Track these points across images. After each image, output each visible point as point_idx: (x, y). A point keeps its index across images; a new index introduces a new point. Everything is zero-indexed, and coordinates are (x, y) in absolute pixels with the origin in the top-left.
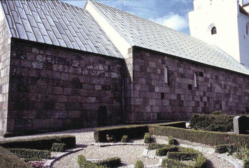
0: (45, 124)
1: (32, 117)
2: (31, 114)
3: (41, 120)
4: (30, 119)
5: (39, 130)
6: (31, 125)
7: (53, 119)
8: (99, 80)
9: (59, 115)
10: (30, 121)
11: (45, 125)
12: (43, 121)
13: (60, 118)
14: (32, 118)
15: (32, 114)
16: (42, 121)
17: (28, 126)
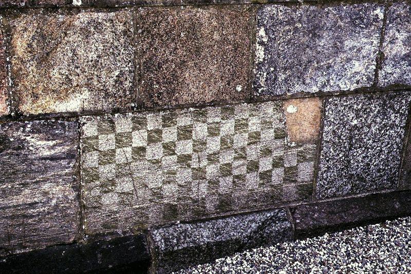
0: (227, 158)
1: (68, 88)
2: (44, 60)
3: (184, 121)
4: (49, 124)
5: (158, 236)
6: (58, 191)
7: (311, 108)
8: (214, 248)
9: (381, 60)
10: (42, 146)
11: (226, 170)
12: (200, 130)
13: (382, 91)
14: (73, 104)
15: (62, 56)
16: (186, 133)
17: (19, 200)
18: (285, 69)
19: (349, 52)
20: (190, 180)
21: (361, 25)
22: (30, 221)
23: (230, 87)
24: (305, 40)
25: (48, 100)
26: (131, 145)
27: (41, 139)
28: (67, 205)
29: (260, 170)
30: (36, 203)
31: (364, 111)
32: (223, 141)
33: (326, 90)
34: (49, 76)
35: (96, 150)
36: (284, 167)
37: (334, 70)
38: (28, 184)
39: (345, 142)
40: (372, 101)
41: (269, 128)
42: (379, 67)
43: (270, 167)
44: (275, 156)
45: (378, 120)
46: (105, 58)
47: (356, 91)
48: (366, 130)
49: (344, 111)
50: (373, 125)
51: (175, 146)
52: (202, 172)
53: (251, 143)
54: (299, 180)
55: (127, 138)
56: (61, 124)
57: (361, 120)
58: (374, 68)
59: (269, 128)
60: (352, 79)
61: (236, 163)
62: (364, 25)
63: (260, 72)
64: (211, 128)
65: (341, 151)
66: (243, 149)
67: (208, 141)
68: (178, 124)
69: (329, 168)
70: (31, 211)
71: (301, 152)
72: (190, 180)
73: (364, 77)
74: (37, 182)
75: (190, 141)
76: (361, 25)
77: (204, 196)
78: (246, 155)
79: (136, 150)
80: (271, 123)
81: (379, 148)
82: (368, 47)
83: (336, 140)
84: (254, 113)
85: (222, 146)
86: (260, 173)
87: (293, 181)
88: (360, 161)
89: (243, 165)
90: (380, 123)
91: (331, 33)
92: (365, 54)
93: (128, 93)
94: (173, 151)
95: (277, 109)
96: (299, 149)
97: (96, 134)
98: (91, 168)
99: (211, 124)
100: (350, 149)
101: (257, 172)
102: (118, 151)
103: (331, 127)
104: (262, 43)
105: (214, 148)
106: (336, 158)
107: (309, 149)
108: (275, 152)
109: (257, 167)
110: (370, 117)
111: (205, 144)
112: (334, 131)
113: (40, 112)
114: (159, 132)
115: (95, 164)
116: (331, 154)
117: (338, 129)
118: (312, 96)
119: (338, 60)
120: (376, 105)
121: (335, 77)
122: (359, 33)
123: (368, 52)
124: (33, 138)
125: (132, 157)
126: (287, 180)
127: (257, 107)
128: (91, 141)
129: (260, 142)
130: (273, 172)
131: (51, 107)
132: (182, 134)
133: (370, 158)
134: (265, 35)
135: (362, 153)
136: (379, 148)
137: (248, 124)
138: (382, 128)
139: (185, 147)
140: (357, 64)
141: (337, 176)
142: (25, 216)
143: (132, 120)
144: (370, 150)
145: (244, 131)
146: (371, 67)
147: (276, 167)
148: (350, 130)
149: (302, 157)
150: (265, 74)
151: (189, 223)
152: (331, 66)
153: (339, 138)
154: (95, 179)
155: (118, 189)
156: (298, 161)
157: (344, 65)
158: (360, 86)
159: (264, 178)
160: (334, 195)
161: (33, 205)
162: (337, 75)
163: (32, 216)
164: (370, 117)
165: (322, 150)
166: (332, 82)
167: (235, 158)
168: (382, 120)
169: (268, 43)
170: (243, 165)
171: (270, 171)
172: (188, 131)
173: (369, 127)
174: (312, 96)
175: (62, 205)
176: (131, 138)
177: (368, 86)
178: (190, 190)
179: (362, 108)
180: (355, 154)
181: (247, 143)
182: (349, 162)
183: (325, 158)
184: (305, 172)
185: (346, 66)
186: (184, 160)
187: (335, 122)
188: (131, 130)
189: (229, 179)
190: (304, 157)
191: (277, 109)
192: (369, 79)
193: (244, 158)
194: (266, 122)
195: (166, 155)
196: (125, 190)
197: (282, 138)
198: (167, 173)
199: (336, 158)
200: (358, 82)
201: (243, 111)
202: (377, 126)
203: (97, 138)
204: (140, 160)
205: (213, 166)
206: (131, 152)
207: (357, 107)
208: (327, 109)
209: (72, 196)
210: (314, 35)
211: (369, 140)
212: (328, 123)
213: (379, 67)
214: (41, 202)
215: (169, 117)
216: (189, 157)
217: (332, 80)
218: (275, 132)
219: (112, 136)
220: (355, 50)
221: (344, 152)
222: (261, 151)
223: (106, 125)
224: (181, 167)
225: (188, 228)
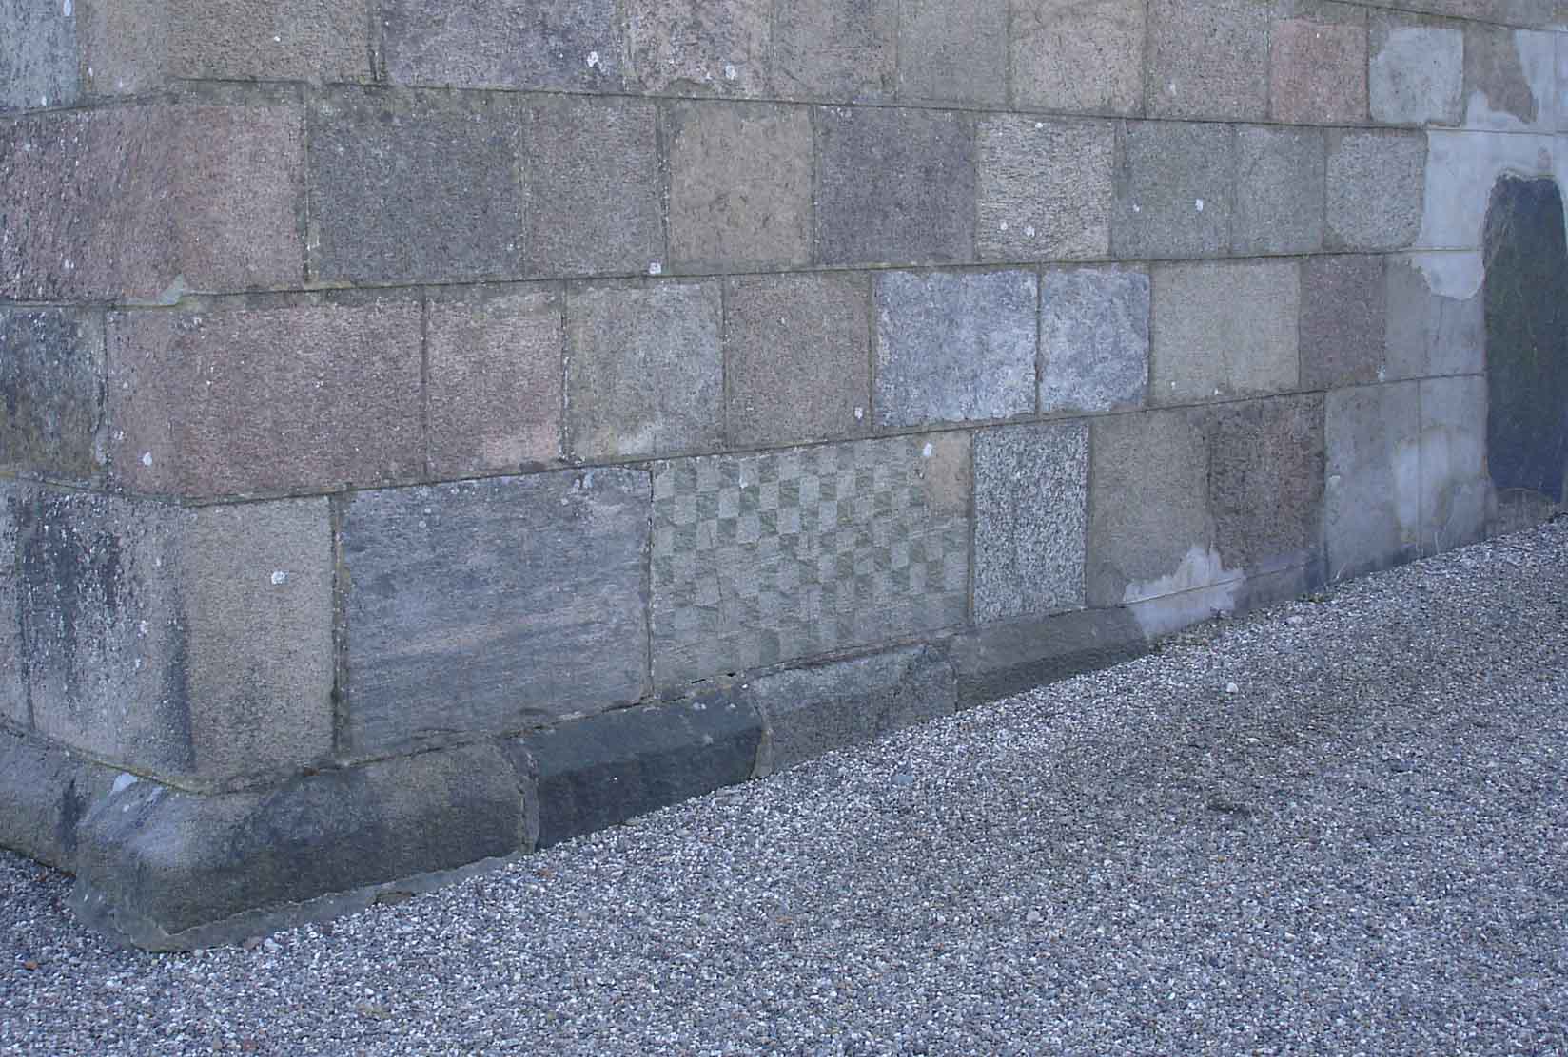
7: (955, 446)
22: (581, 657)
70: (583, 637)
167: (857, 543)
173: (1037, 484)
192: (1029, 399)
210: (952, 321)
223: (685, 477)
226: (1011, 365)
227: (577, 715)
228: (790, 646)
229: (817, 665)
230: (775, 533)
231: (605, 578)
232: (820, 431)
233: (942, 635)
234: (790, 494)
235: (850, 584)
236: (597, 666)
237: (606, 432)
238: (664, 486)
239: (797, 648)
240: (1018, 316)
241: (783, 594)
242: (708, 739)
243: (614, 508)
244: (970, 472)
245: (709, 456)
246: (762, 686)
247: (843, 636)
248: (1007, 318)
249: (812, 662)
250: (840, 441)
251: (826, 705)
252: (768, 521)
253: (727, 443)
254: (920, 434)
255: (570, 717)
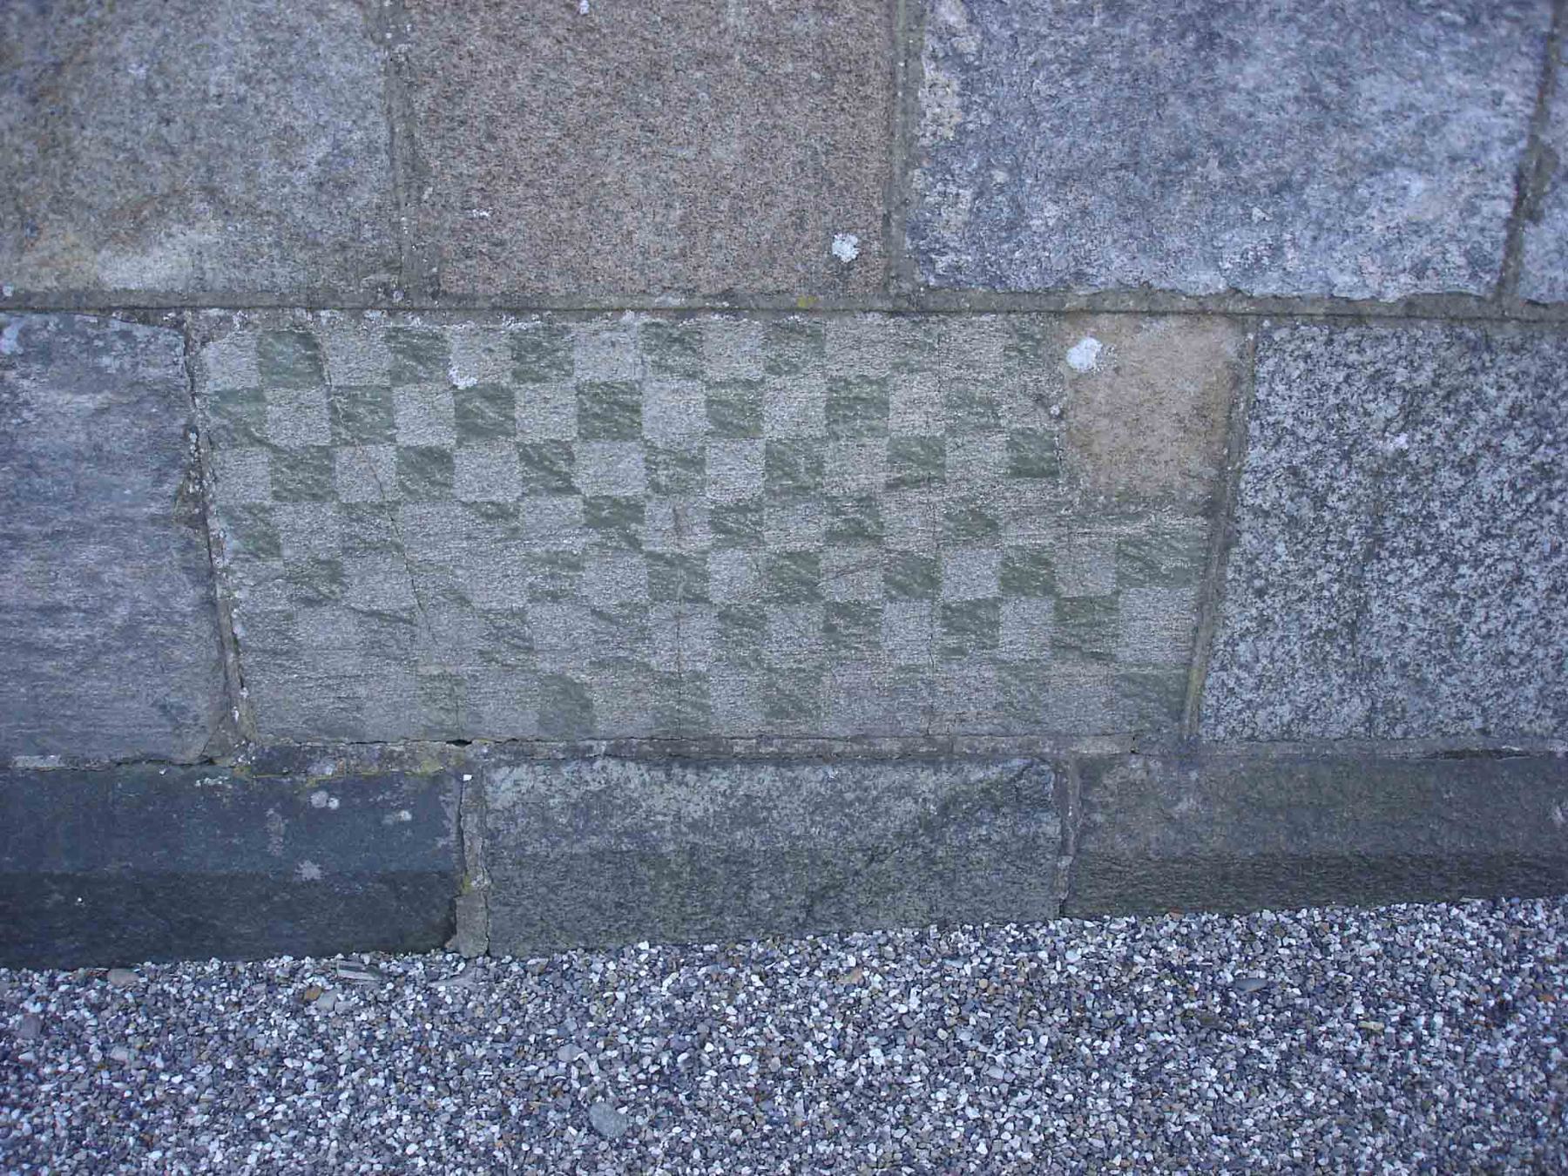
0: (800, 530)
7: (1185, 360)
18: (1065, 179)
19: (1381, 128)
20: (643, 598)
21: (1443, 13)
22: (48, 666)
23: (806, 238)
24: (1166, 56)
25: (72, 238)
26: (392, 439)
27: (61, 386)
28: (168, 630)
29: (947, 594)
30: (60, 608)
31: (1447, 397)
32: (776, 461)
33: (1268, 285)
34: (68, 151)
35: (260, 442)
36: (1058, 595)
37: (1304, 205)
38: (25, 537)
39: (1346, 524)
40: (1486, 357)
41: (983, 427)
42: (1526, 210)
43: (992, 589)
44: (1018, 548)
45: (1512, 443)
46: (272, 88)
47: (1411, 310)
48: (1450, 480)
49: (1345, 388)
50: (1486, 461)
51: (571, 459)
52: (692, 572)
53: (902, 481)
54: (1126, 654)
55: (374, 407)
56: (125, 335)
57: (1430, 437)
58: (1505, 209)
59: (983, 427)
60: (1394, 251)
61: (836, 556)
62: (1461, 12)
63: (940, 187)
64: (720, 402)
65: (1328, 558)
66: (866, 501)
67: (710, 453)
68: (578, 373)
69: (1264, 621)
70: (47, 634)
71: (1136, 542)
72: (643, 598)
73: (1452, 247)
74: (56, 536)
75: (632, 444)
76: (1443, 13)
77: (702, 667)
78: (881, 526)
79: (414, 457)
80: (991, 404)
81: (1510, 566)
82: (1475, 113)
83: (1304, 511)
84: (914, 357)
85: (772, 479)
86: (946, 607)
87: (1097, 657)
88: (1415, 610)
89: (869, 565)
90: (1521, 460)
91: (1292, 37)
92: (1460, 145)
93: (368, 235)
94: (566, 478)
95: (1021, 352)
96: (1127, 530)
97: (254, 384)
98: (248, 509)
99: (722, 384)
100: (1371, 555)
101: (934, 599)
102: (344, 455)
103: (1283, 451)
104: (955, 59)
105: (741, 483)
106: (1301, 584)
107: (1174, 533)
108: (1013, 530)
109: (934, 583)
110: (1474, 428)
111: (697, 463)
112: (1294, 471)
113: (51, 283)
114: (499, 397)
115: (261, 495)
116: (1276, 565)
117: (1315, 463)
118: (1200, 312)
119: (1327, 158)
120: (1506, 380)
121: (1309, 234)
122: (1432, 46)
123: (1479, 138)
124: (25, 376)
125: (401, 484)
126: (1067, 647)
127: (928, 333)
128: (239, 409)
129: (944, 481)
130: (1006, 609)
131: (86, 266)
132: (596, 416)
133: (1462, 601)
134: (963, 25)
135: (1426, 579)
136: (1510, 566)
137: (886, 403)
138: (1531, 482)
139: (612, 470)
140: (1418, 185)
141: (1304, 659)
142: (28, 648)
143: (388, 338)
144: (1463, 569)
145: (871, 429)
146: (1486, 208)
147: (1020, 590)
148: (1378, 475)
149: (1138, 564)
150: (967, 194)
151: (639, 758)
152: (1286, 185)
153: (1319, 502)
154: (263, 550)
155: (357, 596)
156: (1121, 578)
157: (1353, 187)
158: (1430, 285)
159: (963, 630)
160: (1287, 734)
161: (51, 612)
162: (1320, 224)
163: (50, 652)
164: (1474, 428)
165: (1237, 544)
166: (1291, 257)
167: (832, 536)
168: (1534, 445)
169: (979, 58)
170: (869, 565)
171: (994, 604)
172: (625, 407)
173: (1467, 467)
174: (1200, 312)
175: (151, 628)
176: (390, 412)
177: (1472, 288)
178: (643, 635)
179: (1435, 384)
180: (1390, 579)
181: (882, 478)
182: (1362, 608)
183: (1249, 581)
184: (1152, 625)
185: (1363, 192)
186: (614, 518)
187: (1301, 431)
188: (387, 382)
189: (809, 617)
190: (1150, 567)
191: (1021, 352)
192: (1476, 262)
193: (869, 537)
194: (967, 401)
195: (534, 491)
196: (380, 605)
197: (1044, 474)
198: (545, 562)
199: (1301, 584)
200: (1419, 270)
201: (863, 344)
202: (1503, 470)
203: (257, 396)
204: (435, 500)
205: (739, 553)
206: (393, 466)
207: (1410, 379)
208: (1262, 371)
209: (187, 599)
210: (1210, 40)
211: (1464, 524)
212: (1268, 433)
213: (1526, 210)
214: (79, 609)
215: (539, 344)
216: (633, 510)
217: (1295, 244)
218: (1012, 445)
219: (315, 394)
220: (1411, 124)
221: (1339, 562)
222: (948, 516)
223: (287, 351)
224: (601, 545)
225: (628, 780)
226: (1424, 170)
227: (53, 762)
228: (619, 709)
229: (686, 761)
230: (571, 490)
231: (84, 533)
232: (708, 278)
233: (1090, 748)
234: (611, 413)
235: (809, 617)
236: (93, 686)
237: (60, 238)
238: (228, 362)
239: (643, 719)
240: (1466, 41)
241: (598, 614)
242: (310, 871)
243: (88, 402)
244: (1227, 420)
245: (357, 313)
246: (509, 785)
247: (780, 712)
248: (1432, 46)
249: (677, 751)
250: (790, 315)
251: (650, 855)
252: (547, 468)
253: (417, 289)
254: (1058, 314)
255: (36, 762)
